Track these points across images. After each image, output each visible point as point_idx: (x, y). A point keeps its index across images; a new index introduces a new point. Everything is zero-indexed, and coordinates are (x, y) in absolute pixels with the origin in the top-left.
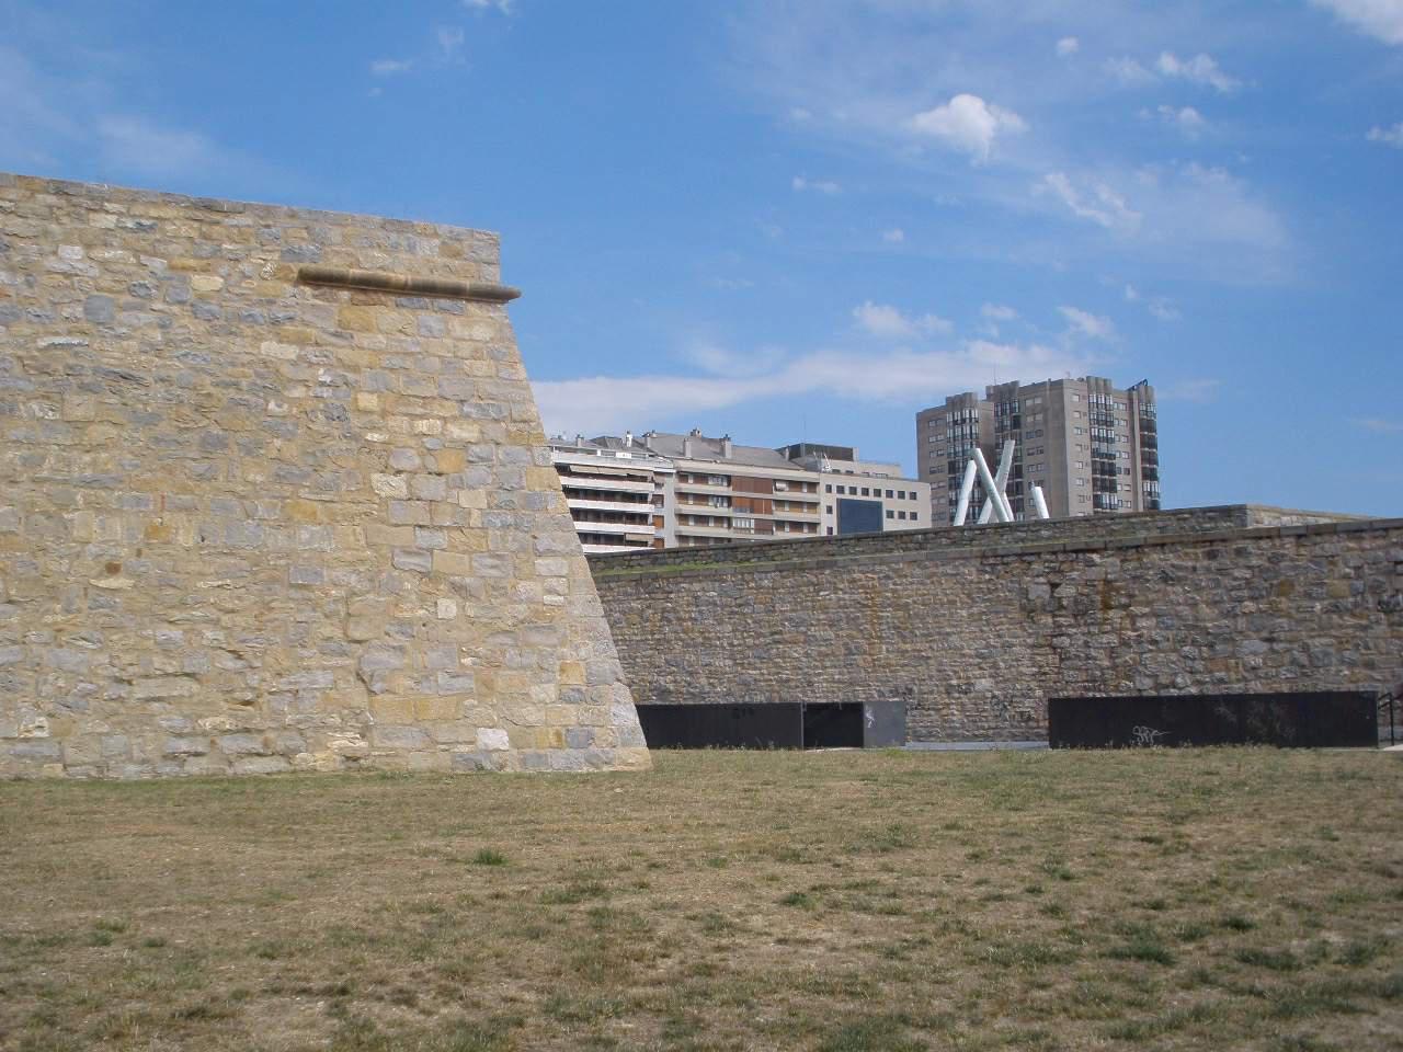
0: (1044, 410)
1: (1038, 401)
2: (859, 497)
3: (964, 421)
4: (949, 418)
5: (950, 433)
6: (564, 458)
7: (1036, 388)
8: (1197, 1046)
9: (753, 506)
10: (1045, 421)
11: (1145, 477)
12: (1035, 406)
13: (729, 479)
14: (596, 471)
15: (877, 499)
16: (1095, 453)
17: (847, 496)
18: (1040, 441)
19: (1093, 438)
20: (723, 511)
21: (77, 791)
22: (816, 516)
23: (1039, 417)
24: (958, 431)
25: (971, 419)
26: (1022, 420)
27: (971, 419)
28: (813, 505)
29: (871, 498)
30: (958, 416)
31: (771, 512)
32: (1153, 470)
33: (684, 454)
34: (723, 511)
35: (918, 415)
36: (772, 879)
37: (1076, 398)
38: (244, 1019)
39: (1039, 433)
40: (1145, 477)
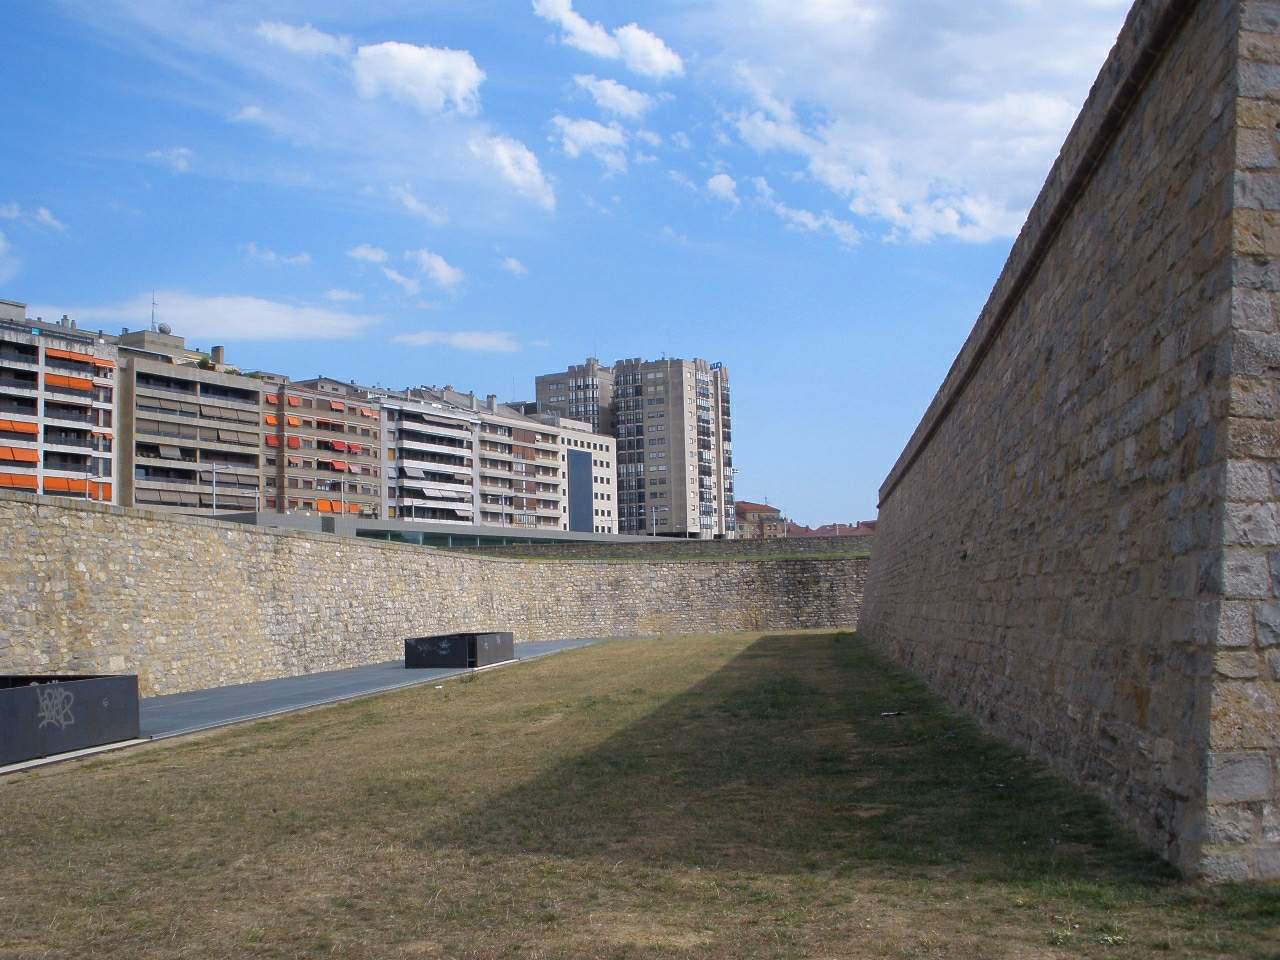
0: (665, 383)
1: (660, 375)
2: (579, 448)
3: (587, 386)
4: (572, 383)
5: (572, 396)
6: (395, 405)
7: (659, 365)
8: (1224, 948)
9: (524, 453)
10: (667, 392)
11: (725, 439)
12: (656, 379)
13: (510, 431)
14: (155, 404)
15: (589, 451)
16: (699, 419)
17: (572, 447)
18: (660, 408)
19: (699, 407)
20: (506, 456)
21: (333, 718)
22: (556, 463)
23: (660, 388)
24: (581, 395)
25: (593, 385)
26: (644, 388)
27: (593, 385)
28: (555, 454)
29: (586, 450)
30: (580, 382)
31: (534, 459)
32: (729, 433)
33: (471, 407)
34: (506, 456)
35: (537, 378)
36: (291, 871)
37: (689, 375)
38: (1205, 862)
39: (660, 401)
40: (725, 439)
